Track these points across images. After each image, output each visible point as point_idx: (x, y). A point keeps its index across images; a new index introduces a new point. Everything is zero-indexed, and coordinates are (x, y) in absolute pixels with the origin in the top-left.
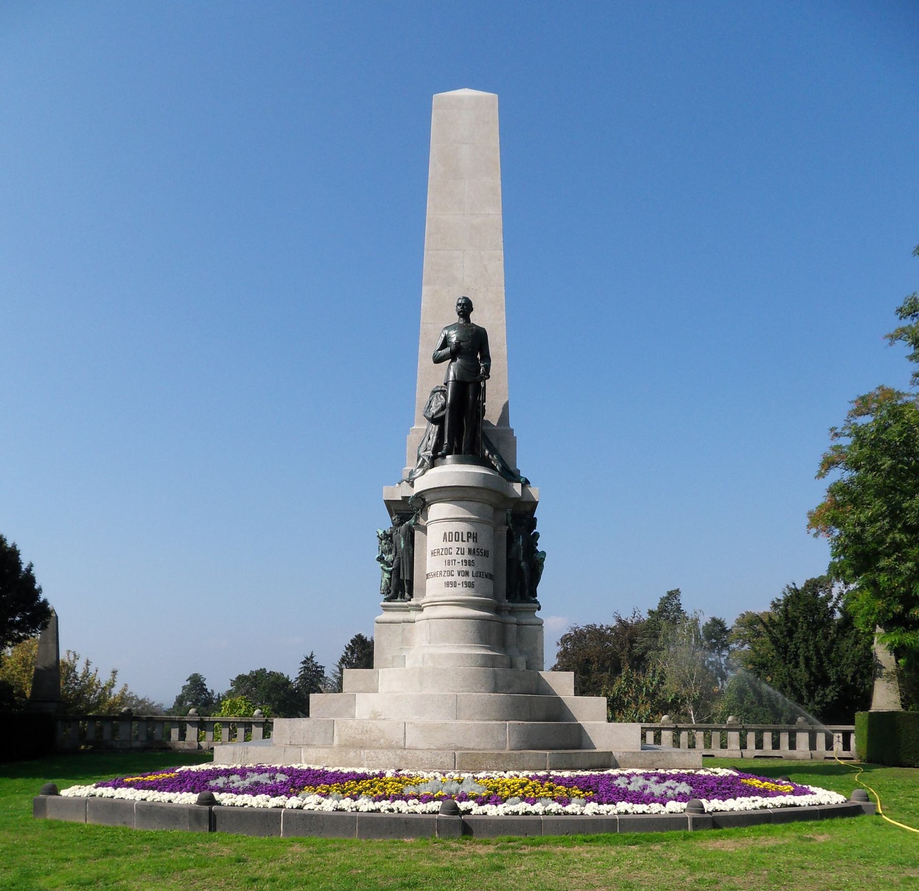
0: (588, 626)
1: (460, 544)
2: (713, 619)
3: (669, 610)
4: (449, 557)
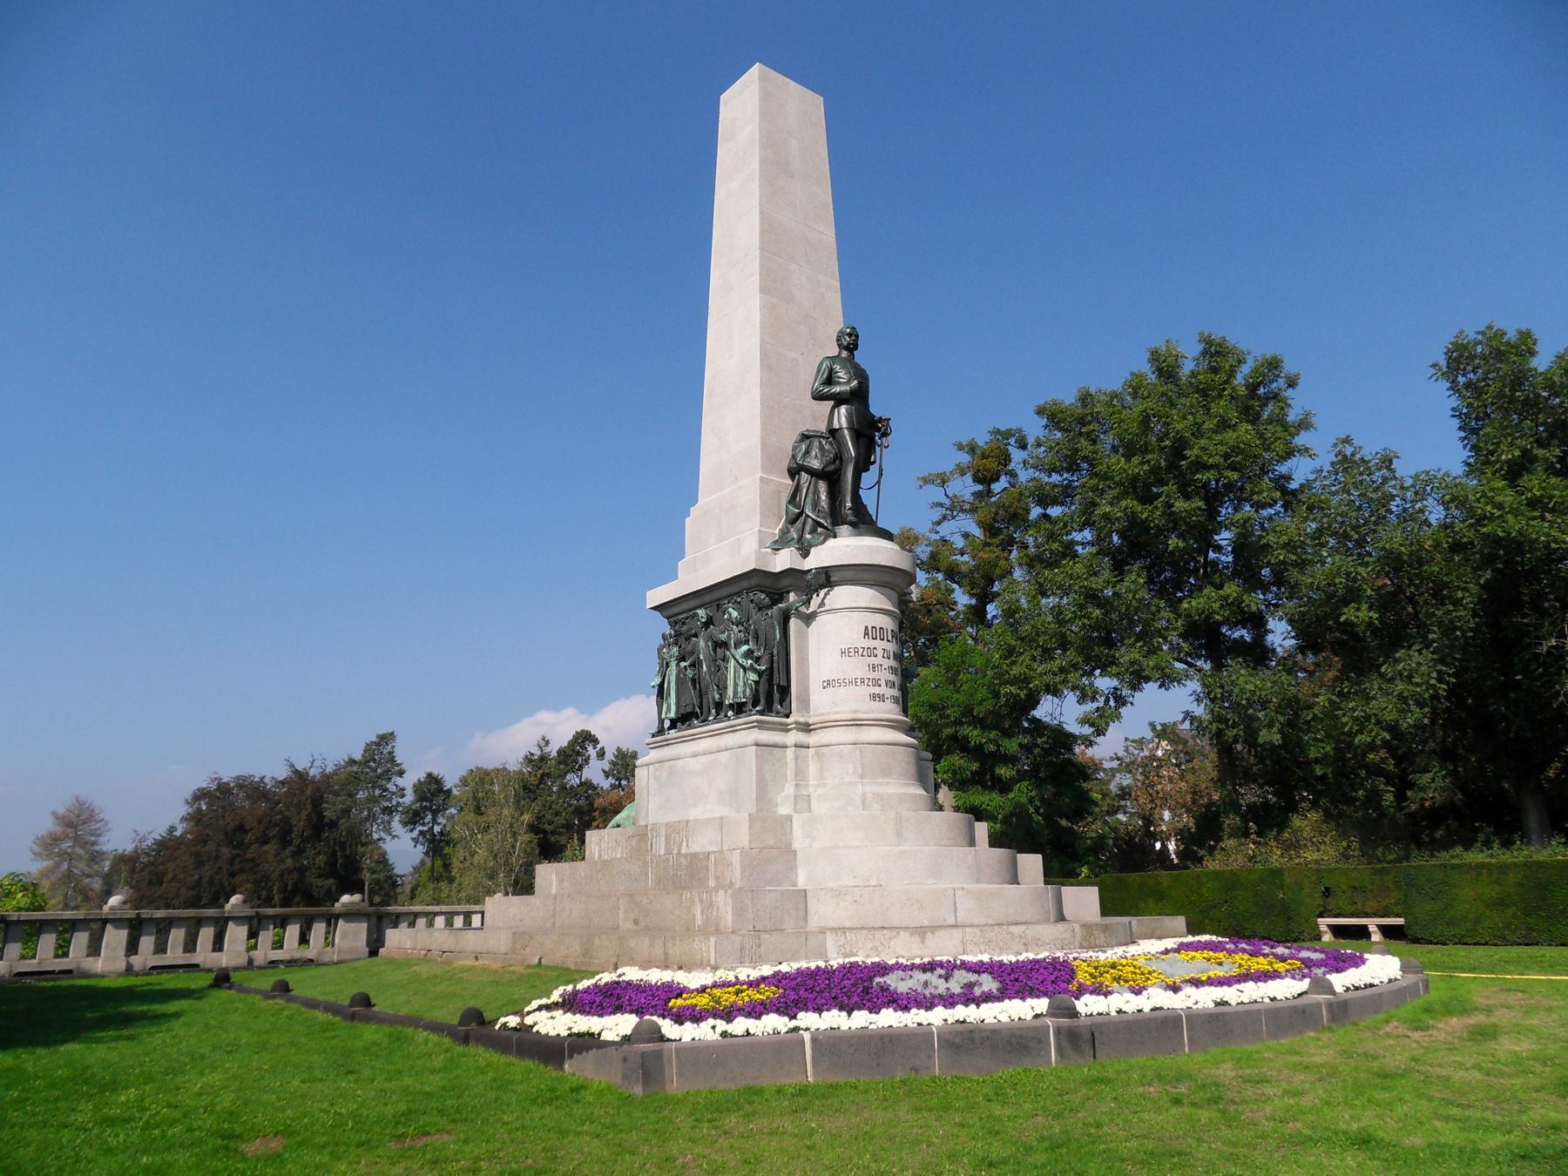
0: (238, 778)
1: (884, 644)
2: (430, 775)
3: (378, 761)
4: (873, 660)
